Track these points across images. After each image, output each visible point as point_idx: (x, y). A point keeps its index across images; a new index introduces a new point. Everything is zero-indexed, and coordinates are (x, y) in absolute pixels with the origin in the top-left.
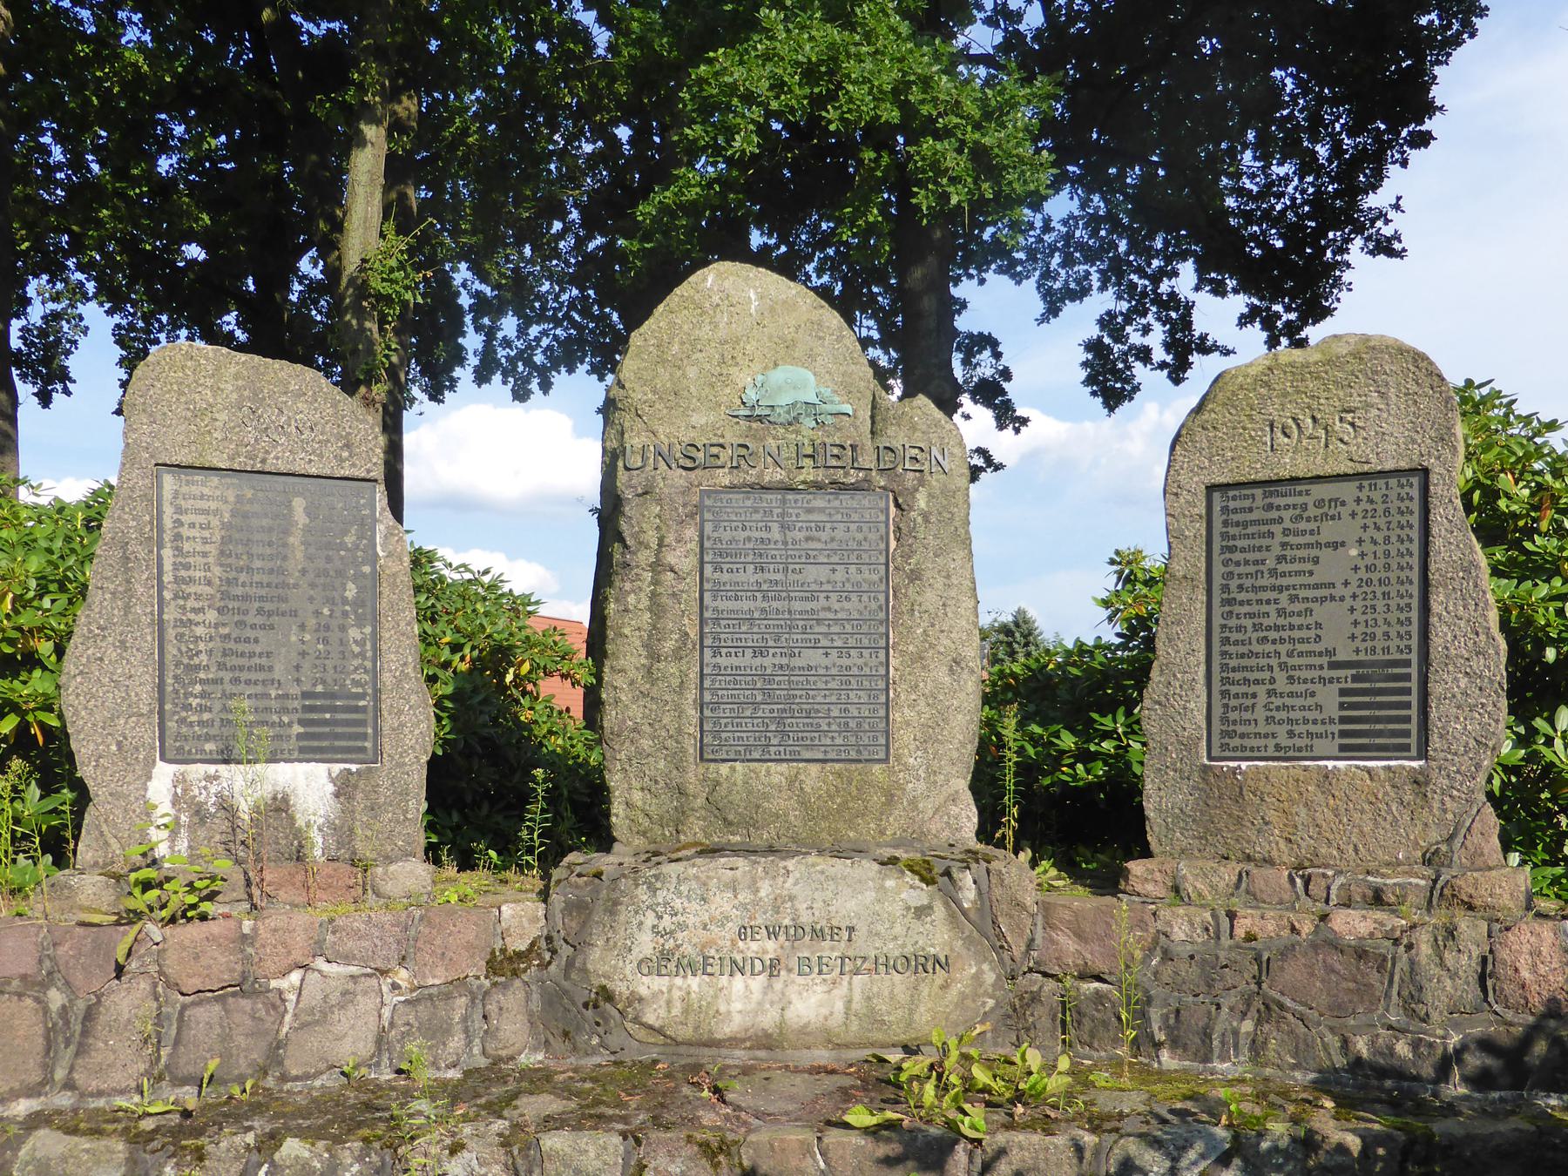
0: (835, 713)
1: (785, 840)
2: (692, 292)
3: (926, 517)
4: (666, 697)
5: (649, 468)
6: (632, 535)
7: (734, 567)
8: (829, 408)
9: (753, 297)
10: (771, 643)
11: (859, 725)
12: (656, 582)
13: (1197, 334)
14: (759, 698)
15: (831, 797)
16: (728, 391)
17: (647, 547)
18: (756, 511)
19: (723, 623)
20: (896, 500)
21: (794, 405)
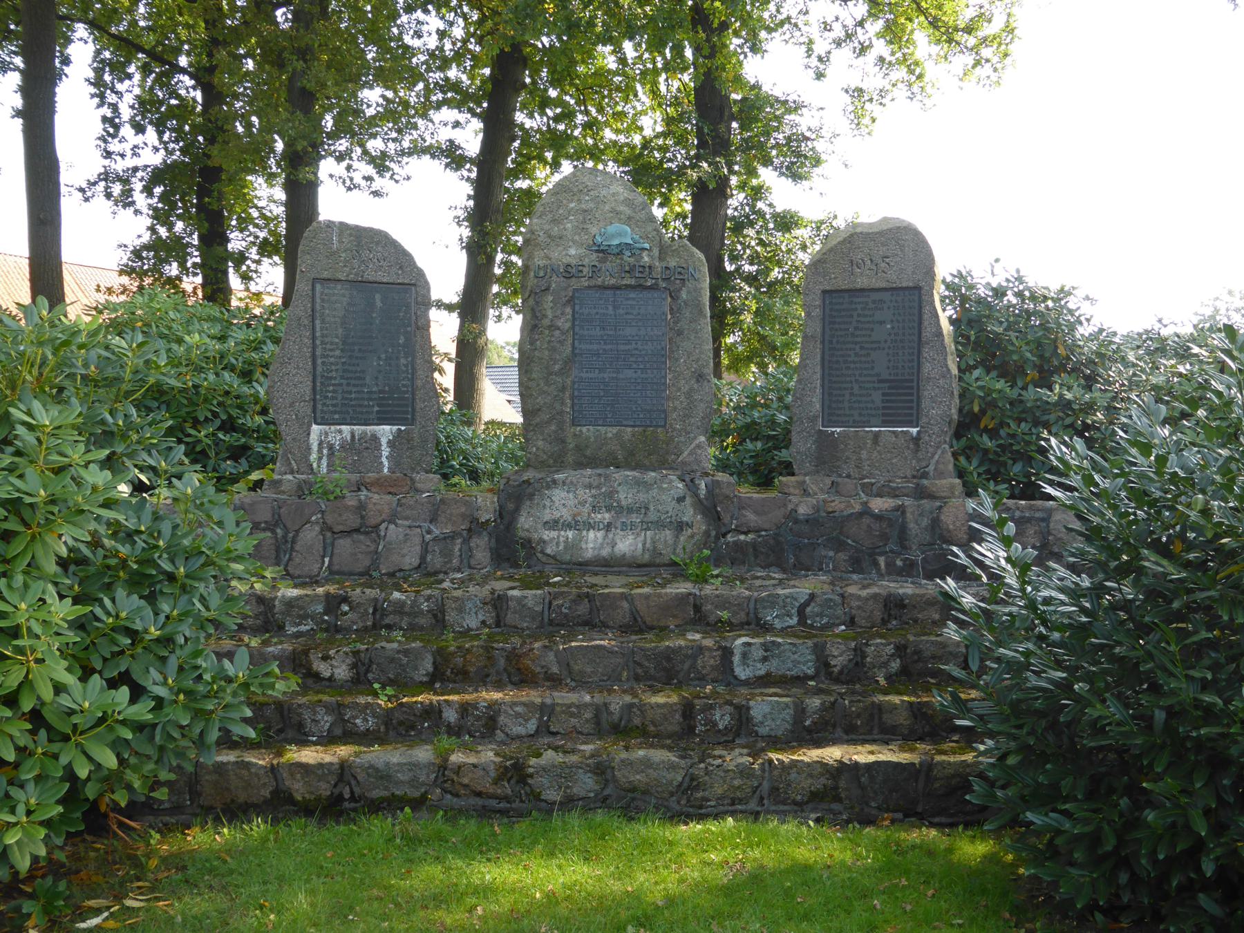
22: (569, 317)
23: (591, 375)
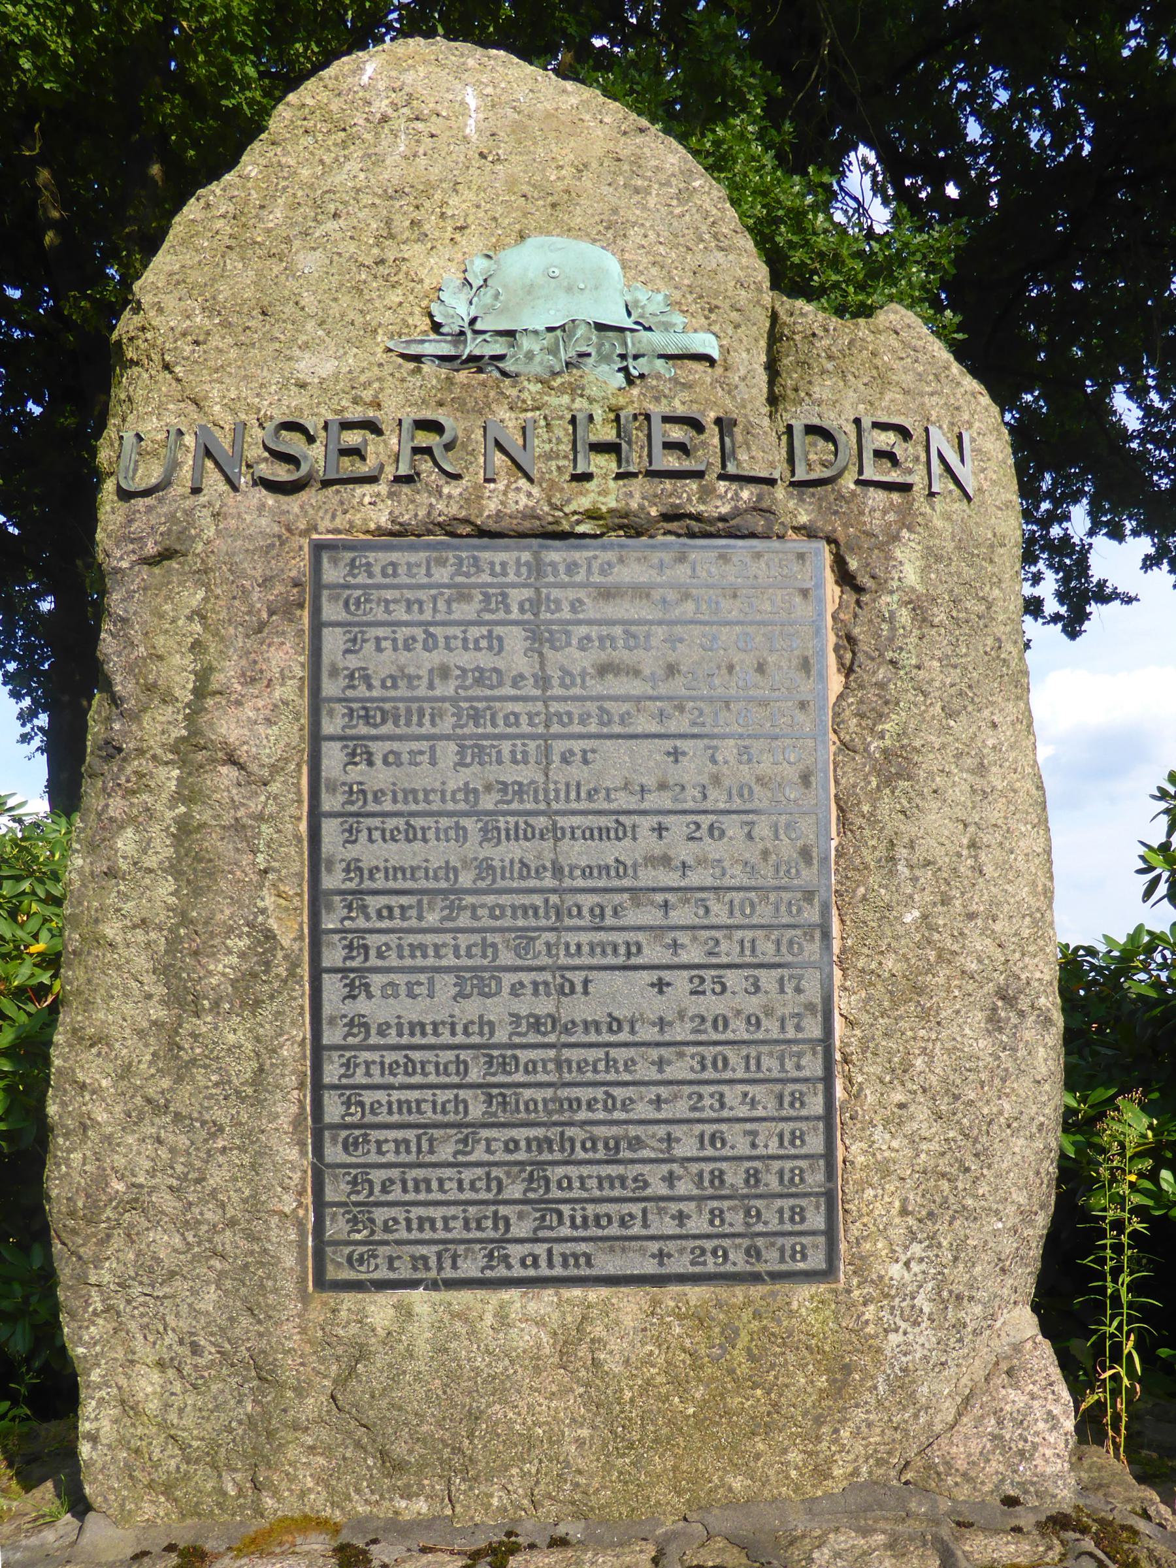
0: (686, 1147)
1: (549, 1509)
2: (324, 96)
3: (919, 607)
4: (218, 1114)
5: (180, 489)
6: (130, 669)
7: (404, 747)
8: (658, 340)
9: (472, 101)
10: (507, 958)
11: (753, 1177)
12: (188, 794)
13: (1095, 580)
14: (476, 1111)
15: (679, 1384)
16: (394, 297)
17: (168, 698)
18: (465, 598)
19: (374, 903)
20: (840, 563)
21: (565, 330)
22: (287, 691)
23: (413, 1011)
